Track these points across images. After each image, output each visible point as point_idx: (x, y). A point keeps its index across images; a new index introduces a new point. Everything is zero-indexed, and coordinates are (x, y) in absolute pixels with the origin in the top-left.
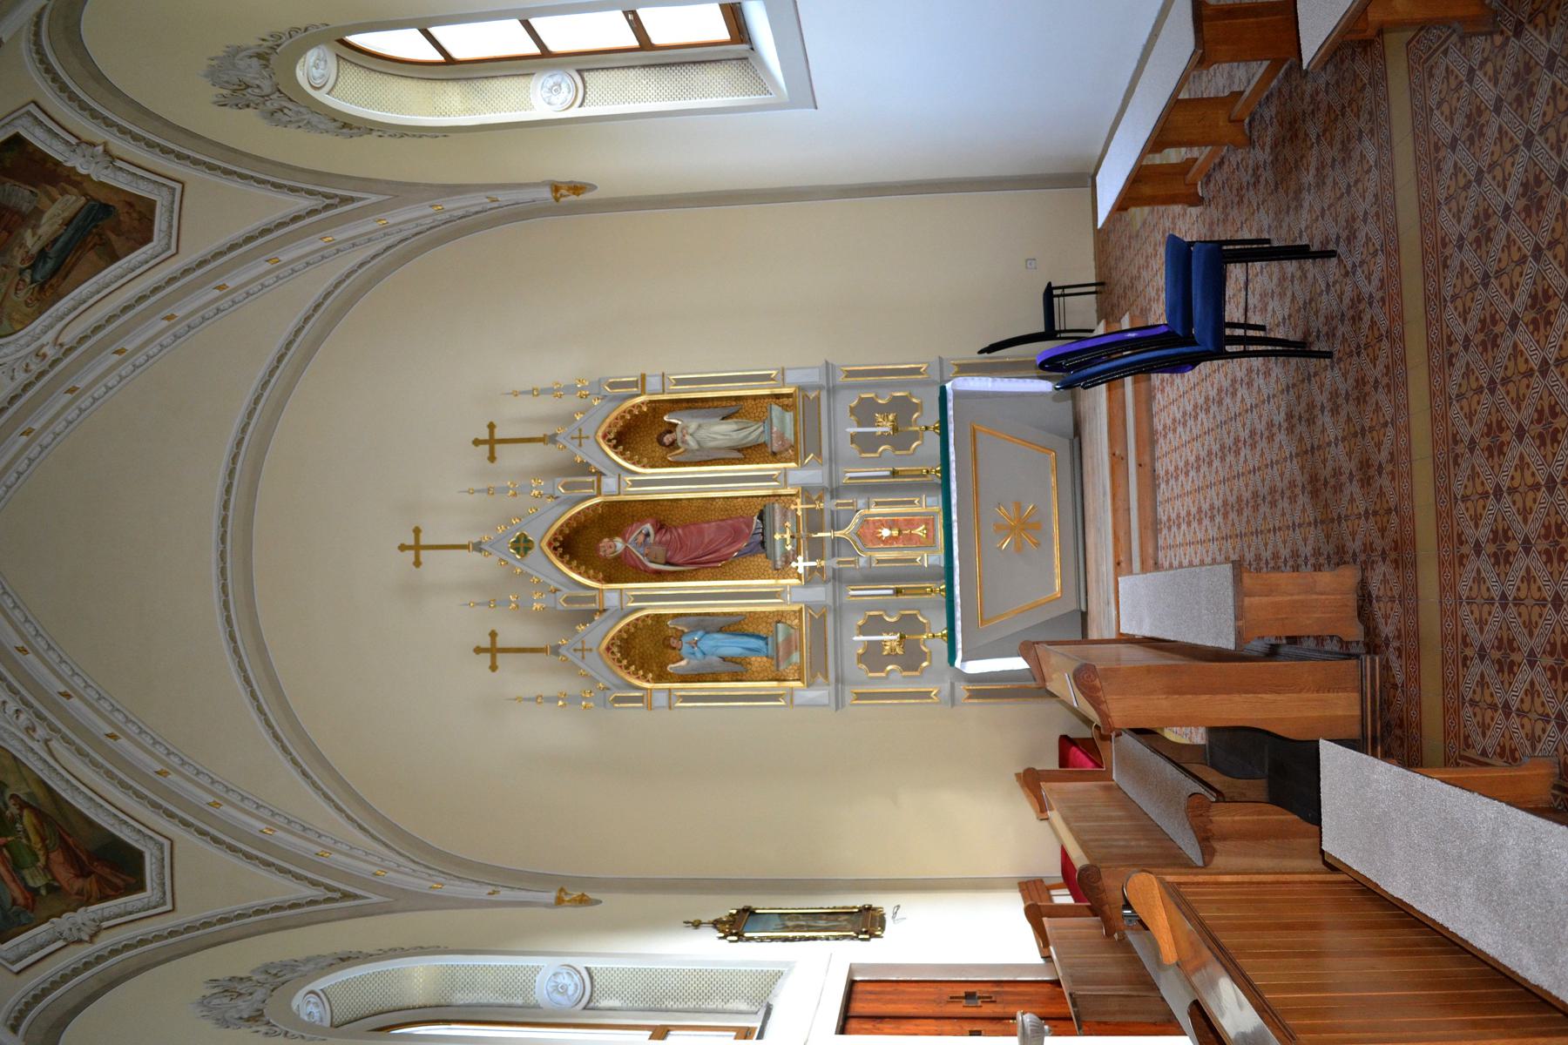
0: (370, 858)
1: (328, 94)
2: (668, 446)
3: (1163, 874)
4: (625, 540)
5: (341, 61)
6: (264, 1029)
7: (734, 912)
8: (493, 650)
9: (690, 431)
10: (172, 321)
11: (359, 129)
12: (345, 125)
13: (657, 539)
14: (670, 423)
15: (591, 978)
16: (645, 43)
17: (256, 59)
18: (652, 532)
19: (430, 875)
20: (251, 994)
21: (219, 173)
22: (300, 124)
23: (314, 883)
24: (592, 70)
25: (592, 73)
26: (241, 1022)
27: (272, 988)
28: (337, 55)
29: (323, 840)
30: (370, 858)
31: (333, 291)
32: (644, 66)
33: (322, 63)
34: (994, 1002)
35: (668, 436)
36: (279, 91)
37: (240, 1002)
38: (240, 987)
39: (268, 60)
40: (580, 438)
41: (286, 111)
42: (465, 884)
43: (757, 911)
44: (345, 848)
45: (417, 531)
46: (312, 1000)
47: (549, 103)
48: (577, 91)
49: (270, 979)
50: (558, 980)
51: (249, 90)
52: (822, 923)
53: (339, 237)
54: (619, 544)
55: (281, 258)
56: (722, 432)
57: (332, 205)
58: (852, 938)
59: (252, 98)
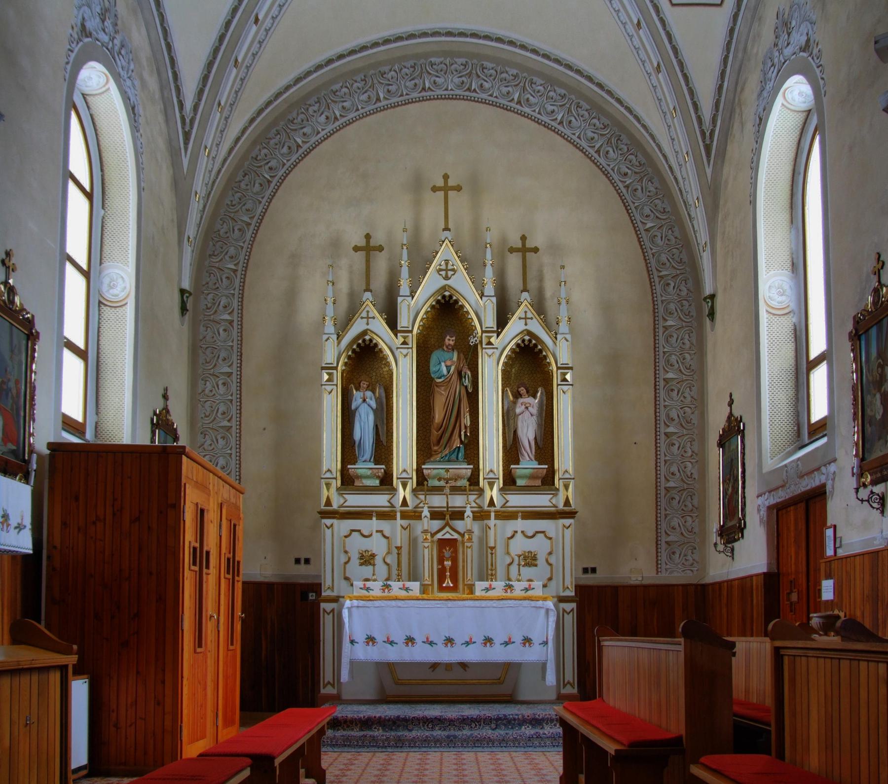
1: (783, 105)
2: (518, 391)
3: (207, 616)
5: (805, 114)
7: (175, 427)
8: (369, 248)
12: (761, 119)
16: (812, 365)
17: (806, 38)
21: (731, 25)
22: (763, 83)
23: (196, 108)
27: (109, 47)
28: (810, 111)
35: (525, 390)
36: (785, 61)
38: (108, 23)
39: (804, 51)
40: (526, 318)
41: (773, 68)
42: (202, 202)
45: (458, 188)
46: (101, 81)
47: (770, 286)
49: (117, 48)
51: (787, 36)
55: (641, 30)
56: (528, 431)
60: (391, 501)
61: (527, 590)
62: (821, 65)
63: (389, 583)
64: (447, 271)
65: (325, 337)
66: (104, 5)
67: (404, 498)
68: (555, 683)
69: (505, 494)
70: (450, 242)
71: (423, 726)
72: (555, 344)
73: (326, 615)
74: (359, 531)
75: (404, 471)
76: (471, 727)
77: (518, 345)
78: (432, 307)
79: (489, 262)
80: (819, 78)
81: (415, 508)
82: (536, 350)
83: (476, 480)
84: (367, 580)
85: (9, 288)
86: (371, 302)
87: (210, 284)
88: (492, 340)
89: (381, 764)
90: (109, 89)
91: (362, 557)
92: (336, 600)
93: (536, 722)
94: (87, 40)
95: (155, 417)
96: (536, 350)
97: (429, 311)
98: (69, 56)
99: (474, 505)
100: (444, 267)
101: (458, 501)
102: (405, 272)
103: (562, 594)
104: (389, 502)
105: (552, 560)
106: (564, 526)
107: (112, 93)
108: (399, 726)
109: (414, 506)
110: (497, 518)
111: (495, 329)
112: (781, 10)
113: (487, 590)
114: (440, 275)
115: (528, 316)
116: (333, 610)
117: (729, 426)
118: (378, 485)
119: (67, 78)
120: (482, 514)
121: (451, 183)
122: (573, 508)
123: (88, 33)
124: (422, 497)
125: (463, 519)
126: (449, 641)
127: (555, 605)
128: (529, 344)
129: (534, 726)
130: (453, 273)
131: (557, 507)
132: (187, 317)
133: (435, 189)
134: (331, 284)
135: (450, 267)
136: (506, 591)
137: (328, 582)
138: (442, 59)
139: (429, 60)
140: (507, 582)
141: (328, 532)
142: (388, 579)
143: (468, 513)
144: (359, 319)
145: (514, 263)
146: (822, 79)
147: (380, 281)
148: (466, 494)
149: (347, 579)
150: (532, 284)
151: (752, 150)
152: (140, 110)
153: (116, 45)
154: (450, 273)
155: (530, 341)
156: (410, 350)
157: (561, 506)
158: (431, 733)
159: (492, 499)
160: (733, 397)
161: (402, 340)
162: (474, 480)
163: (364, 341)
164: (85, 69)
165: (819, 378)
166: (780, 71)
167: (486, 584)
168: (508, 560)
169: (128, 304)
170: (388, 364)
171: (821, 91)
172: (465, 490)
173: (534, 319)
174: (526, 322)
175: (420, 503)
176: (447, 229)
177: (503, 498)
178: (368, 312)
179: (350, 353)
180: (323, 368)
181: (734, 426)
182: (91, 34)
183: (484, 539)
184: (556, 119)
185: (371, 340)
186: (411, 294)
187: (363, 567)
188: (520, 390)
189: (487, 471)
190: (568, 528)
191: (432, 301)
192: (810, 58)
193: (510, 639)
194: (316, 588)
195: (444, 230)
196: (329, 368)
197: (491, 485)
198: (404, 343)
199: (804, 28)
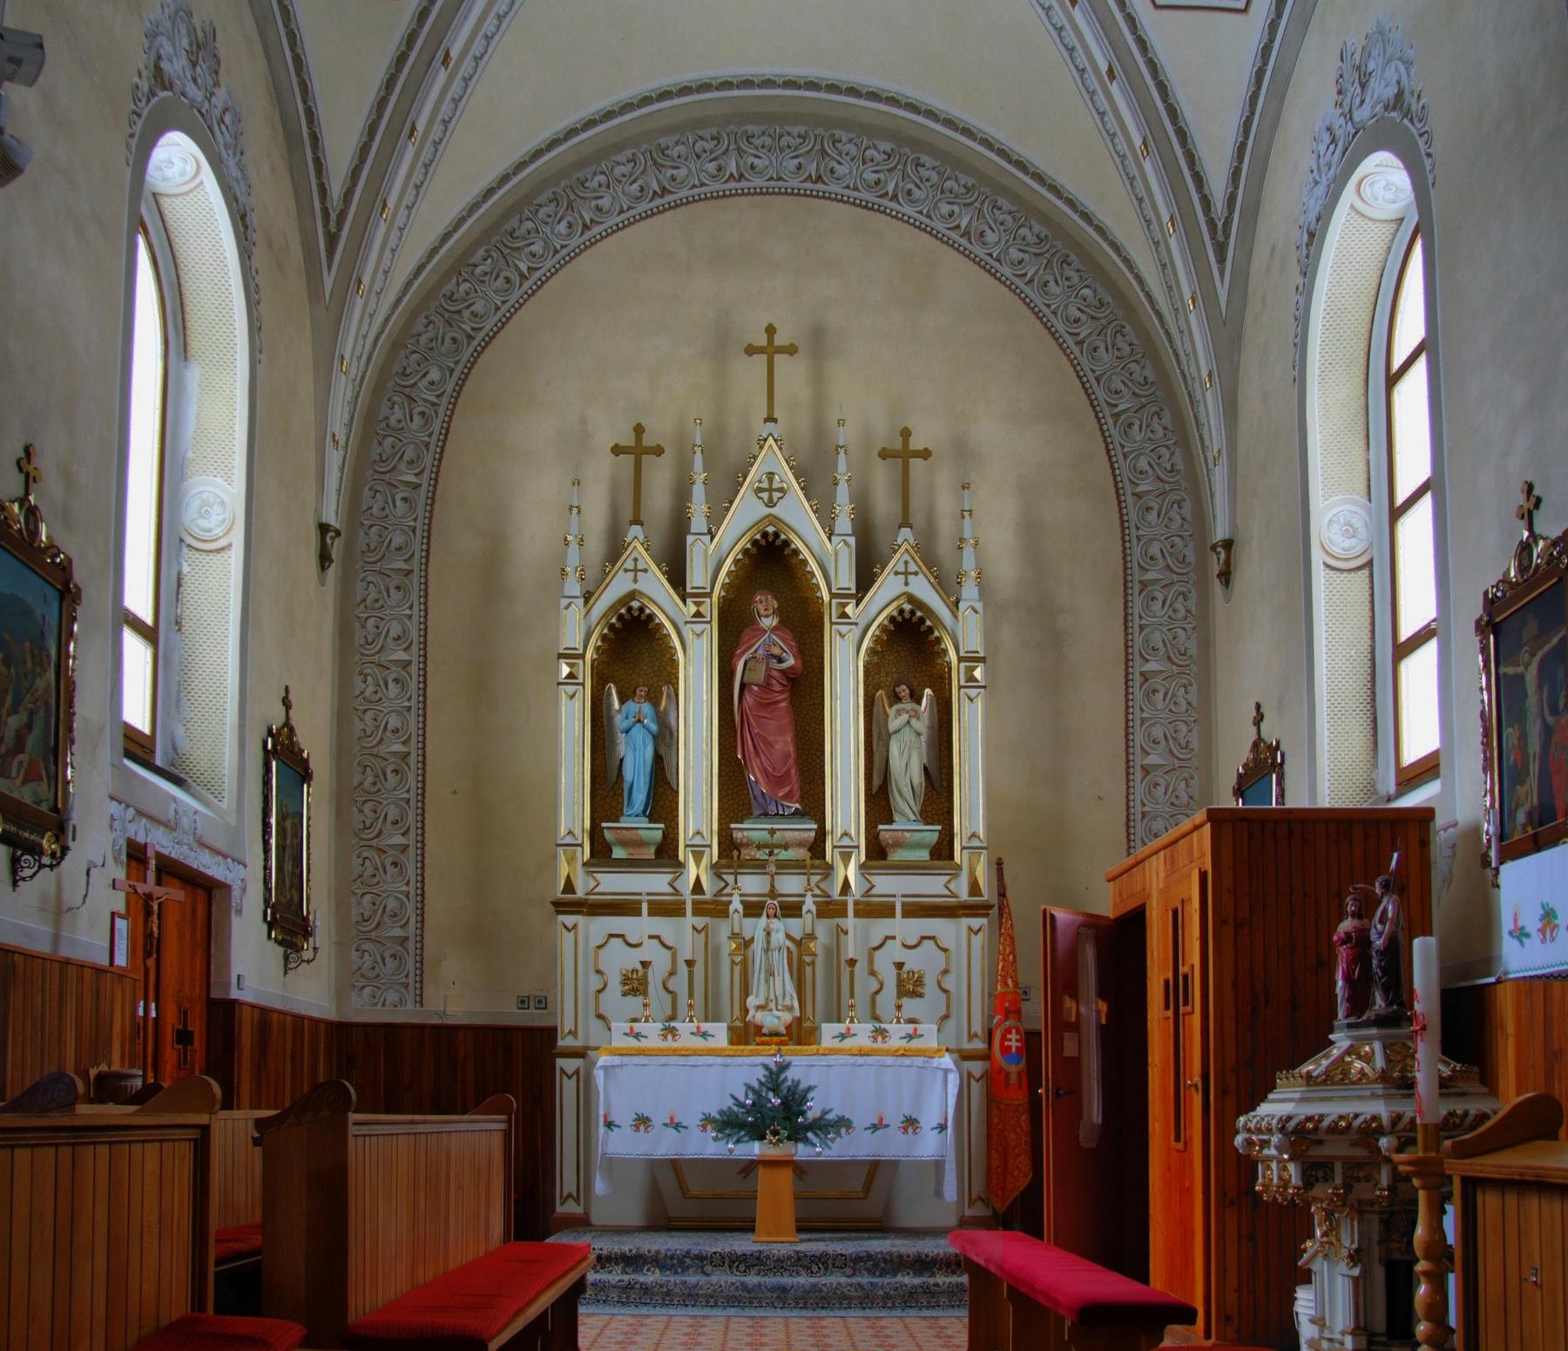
0: (380, 275)
1: (1352, 206)
2: (894, 691)
4: (774, 630)
6: (144, 86)
7: (305, 755)
8: (638, 450)
9: (913, 721)
10: (1106, 77)
11: (1307, 257)
12: (1312, 235)
13: (775, 673)
14: (922, 697)
15: (218, 551)
18: (784, 666)
19: (359, 358)
20: (195, 80)
23: (348, 196)
24: (1372, 581)
25: (1367, 580)
26: (153, 56)
27: (203, 111)
28: (1401, 220)
29: (403, 212)
30: (380, 275)
31: (1106, 239)
32: (1373, 652)
33: (1392, 196)
34: (179, 1067)
35: (907, 691)
36: (1356, 133)
37: (184, 61)
39: (1394, 109)
40: (906, 573)
42: (347, 409)
43: (305, 786)
44: (392, 242)
45: (791, 350)
46: (188, 168)
47: (1330, 521)
48: (1345, 560)
49: (216, 113)
50: (215, 507)
51: (1359, 90)
52: (288, 866)
53: (1173, 243)
54: (768, 622)
57: (1216, 232)
58: (267, 901)
59: (1349, 96)
60: (675, 884)
61: (910, 1037)
62: (1426, 132)
63: (672, 1024)
64: (770, 492)
65: (565, 602)
66: (197, 37)
67: (698, 880)
68: (955, 1199)
69: (869, 874)
70: (776, 441)
71: (730, 1267)
72: (956, 617)
73: (565, 1078)
74: (622, 936)
75: (698, 833)
76: (812, 1272)
77: (892, 619)
78: (745, 552)
79: (843, 480)
80: (1423, 153)
81: (715, 896)
82: (923, 628)
83: (820, 849)
84: (635, 1020)
85: (28, 509)
86: (642, 544)
87: (375, 511)
88: (849, 610)
89: (628, 1325)
90: (202, 183)
91: (626, 980)
92: (580, 1053)
93: (923, 1264)
94: (163, 94)
95: (270, 740)
96: (923, 628)
97: (739, 560)
98: (135, 123)
99: (817, 892)
100: (765, 485)
101: (791, 884)
102: (698, 493)
103: (966, 1046)
104: (671, 885)
105: (949, 983)
106: (970, 929)
107: (208, 190)
108: (689, 1267)
109: (715, 892)
110: (857, 914)
111: (854, 591)
112: (1349, 45)
113: (843, 1036)
114: (760, 498)
115: (910, 570)
116: (577, 1072)
117: (1254, 759)
118: (653, 857)
119: (131, 162)
120: (831, 907)
121: (780, 340)
122: (986, 898)
123: (167, 83)
124: (730, 879)
125: (800, 916)
126: (642, 1122)
127: (955, 1063)
128: (911, 618)
129: (918, 1273)
130: (781, 495)
131: (957, 897)
132: (332, 571)
133: (751, 350)
134: (575, 511)
135: (775, 485)
136: (875, 1039)
137: (568, 1025)
138: (764, 128)
139: (744, 128)
140: (877, 1025)
141: (568, 938)
142: (673, 1018)
143: (809, 904)
144: (621, 572)
145: (882, 478)
146: (1429, 155)
147: (658, 499)
148: (805, 874)
149: (600, 1017)
150: (918, 518)
151: (1297, 289)
152: (254, 219)
153: (215, 106)
154: (776, 495)
155: (913, 613)
156: (708, 626)
157: (964, 895)
158: (742, 1279)
159: (846, 882)
160: (1261, 710)
161: (693, 609)
162: (817, 847)
163: (630, 609)
164: (162, 146)
165: (1420, 673)
166: (1347, 150)
167: (841, 1028)
168: (875, 986)
169: (233, 549)
170: (671, 651)
171: (1426, 177)
172: (804, 867)
173: (921, 576)
174: (906, 579)
175: (724, 888)
176: (770, 419)
177: (865, 880)
178: (636, 560)
179: (614, 620)
180: (561, 656)
181: (1266, 759)
182: (171, 85)
183: (834, 951)
184: (958, 227)
185: (641, 610)
186: (710, 529)
187: (630, 998)
188: (897, 690)
189: (839, 835)
190: (976, 933)
191: (744, 543)
192: (1406, 121)
193: (881, 1120)
194: (551, 1033)
195: (766, 420)
196: (571, 656)
197: (846, 858)
198: (698, 614)
199: (1391, 75)
